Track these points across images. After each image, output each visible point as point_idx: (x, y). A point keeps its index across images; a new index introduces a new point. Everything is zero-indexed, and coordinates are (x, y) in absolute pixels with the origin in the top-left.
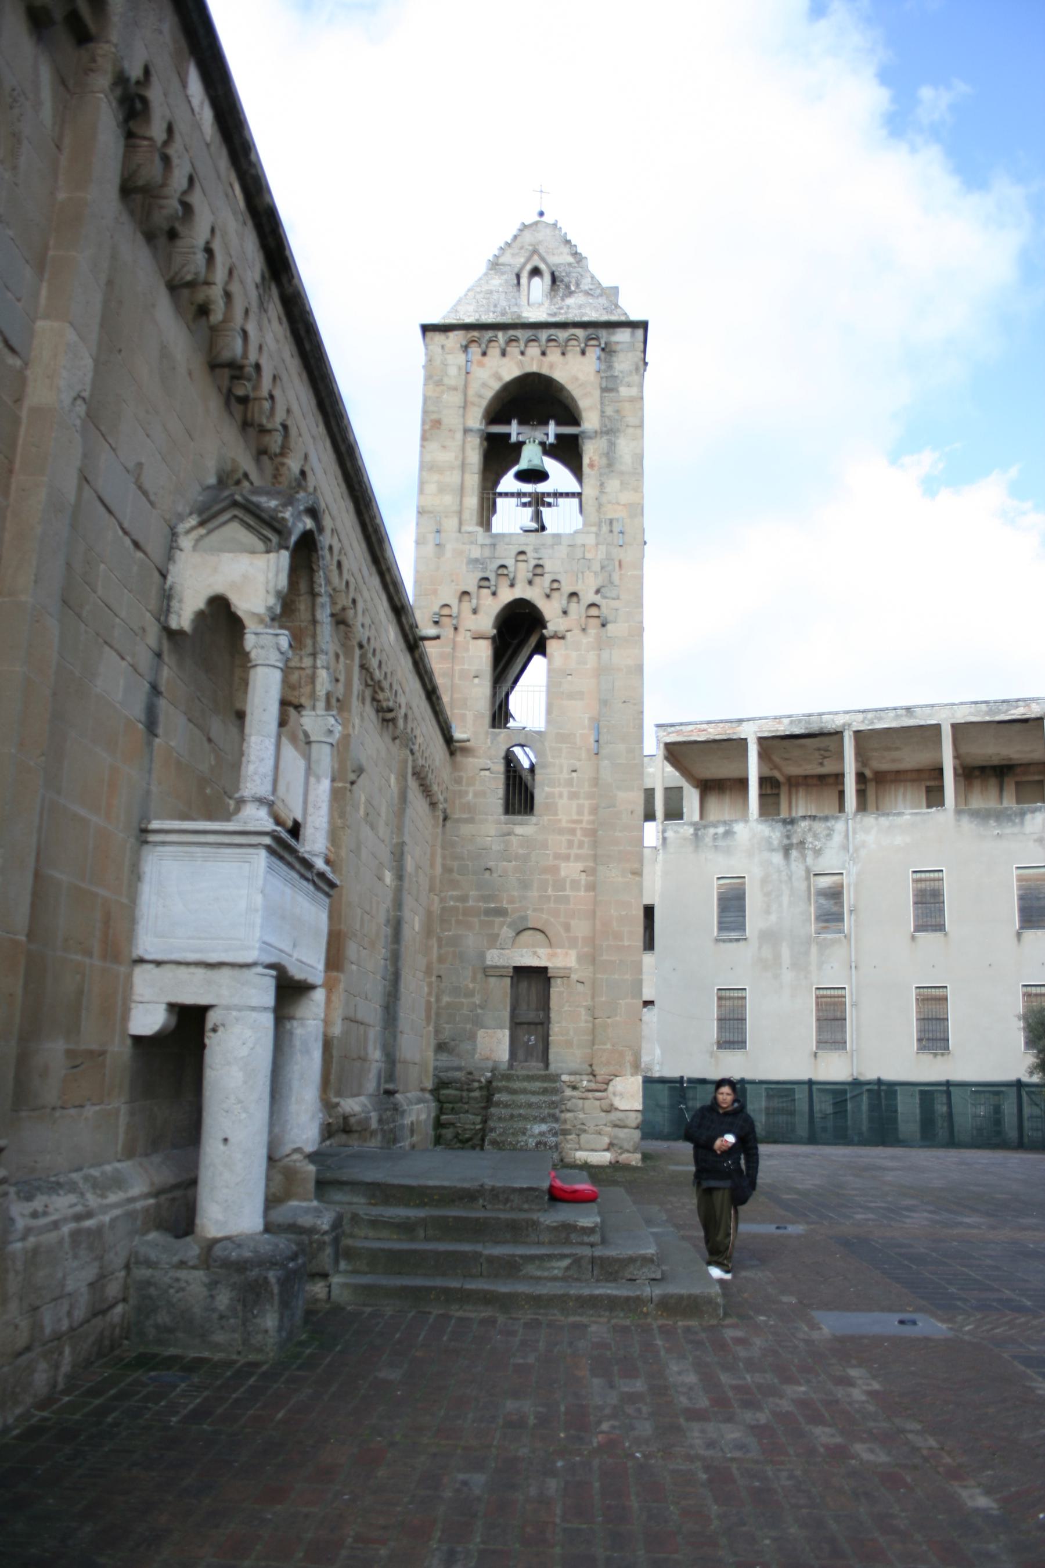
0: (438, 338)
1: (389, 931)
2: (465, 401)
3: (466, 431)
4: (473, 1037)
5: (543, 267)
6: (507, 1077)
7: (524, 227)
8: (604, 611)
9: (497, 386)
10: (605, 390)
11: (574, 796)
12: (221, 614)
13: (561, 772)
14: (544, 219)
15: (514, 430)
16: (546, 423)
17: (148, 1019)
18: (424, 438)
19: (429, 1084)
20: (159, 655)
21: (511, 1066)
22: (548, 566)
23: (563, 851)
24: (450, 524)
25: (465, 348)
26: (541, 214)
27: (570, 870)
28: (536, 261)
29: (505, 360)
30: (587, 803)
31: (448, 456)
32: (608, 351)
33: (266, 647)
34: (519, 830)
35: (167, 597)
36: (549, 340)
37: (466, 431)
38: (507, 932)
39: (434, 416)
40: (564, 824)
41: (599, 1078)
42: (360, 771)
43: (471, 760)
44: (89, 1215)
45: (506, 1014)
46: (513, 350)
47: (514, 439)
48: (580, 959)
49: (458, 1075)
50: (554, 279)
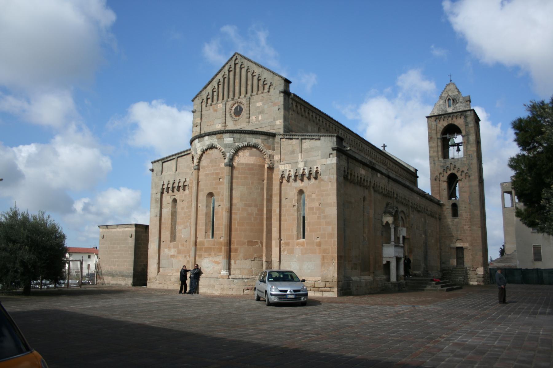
0: (430, 119)
3: (438, 138)
6: (456, 268)
7: (447, 85)
8: (469, 174)
9: (443, 127)
10: (466, 126)
11: (466, 212)
12: (387, 223)
15: (448, 136)
17: (384, 262)
18: (429, 141)
19: (439, 270)
21: (457, 266)
22: (457, 166)
24: (436, 159)
25: (436, 121)
27: (466, 227)
28: (449, 97)
31: (434, 145)
32: (466, 117)
33: (392, 227)
35: (382, 222)
37: (438, 138)
45: (455, 256)
46: (446, 119)
50: (453, 100)
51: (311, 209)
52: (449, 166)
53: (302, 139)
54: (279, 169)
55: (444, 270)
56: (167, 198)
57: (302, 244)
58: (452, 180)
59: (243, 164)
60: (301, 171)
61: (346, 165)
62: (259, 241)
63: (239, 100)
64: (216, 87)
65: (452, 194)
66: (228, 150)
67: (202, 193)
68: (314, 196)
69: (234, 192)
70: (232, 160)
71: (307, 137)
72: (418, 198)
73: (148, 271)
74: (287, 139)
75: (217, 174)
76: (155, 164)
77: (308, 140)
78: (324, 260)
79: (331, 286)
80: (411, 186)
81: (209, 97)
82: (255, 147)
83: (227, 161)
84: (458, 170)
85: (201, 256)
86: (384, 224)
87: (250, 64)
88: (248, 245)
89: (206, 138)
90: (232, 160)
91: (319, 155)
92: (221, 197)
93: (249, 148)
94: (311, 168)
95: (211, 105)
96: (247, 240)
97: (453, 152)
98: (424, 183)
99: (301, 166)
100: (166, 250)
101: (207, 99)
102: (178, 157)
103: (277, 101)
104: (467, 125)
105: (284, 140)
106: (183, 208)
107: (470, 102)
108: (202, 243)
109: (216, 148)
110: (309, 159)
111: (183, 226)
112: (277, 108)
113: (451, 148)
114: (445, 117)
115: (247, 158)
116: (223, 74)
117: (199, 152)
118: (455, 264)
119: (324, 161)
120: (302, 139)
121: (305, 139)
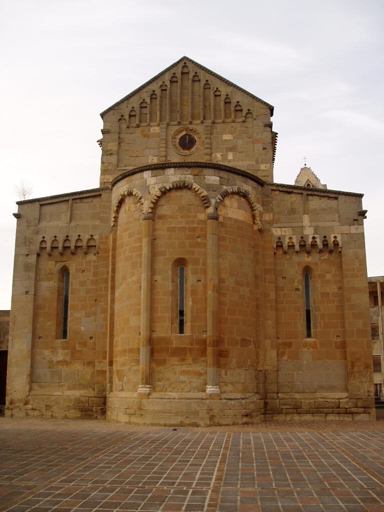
5: (310, 184)
26: (305, 165)
28: (308, 183)
53: (308, 195)
56: (51, 266)
57: (314, 346)
59: (230, 219)
60: (310, 240)
63: (191, 127)
64: (148, 100)
66: (212, 194)
67: (162, 258)
71: (316, 193)
73: (8, 387)
75: (193, 230)
76: (25, 206)
82: (245, 196)
85: (163, 362)
87: (210, 78)
88: (242, 346)
89: (172, 171)
92: (201, 266)
93: (237, 197)
95: (138, 126)
100: (47, 352)
102: (73, 199)
103: (260, 136)
105: (277, 193)
106: (83, 284)
108: (166, 340)
109: (190, 189)
110: (321, 224)
111: (83, 313)
112: (259, 147)
116: (161, 83)
117: (155, 191)
119: (345, 229)
120: (308, 195)
121: (312, 195)
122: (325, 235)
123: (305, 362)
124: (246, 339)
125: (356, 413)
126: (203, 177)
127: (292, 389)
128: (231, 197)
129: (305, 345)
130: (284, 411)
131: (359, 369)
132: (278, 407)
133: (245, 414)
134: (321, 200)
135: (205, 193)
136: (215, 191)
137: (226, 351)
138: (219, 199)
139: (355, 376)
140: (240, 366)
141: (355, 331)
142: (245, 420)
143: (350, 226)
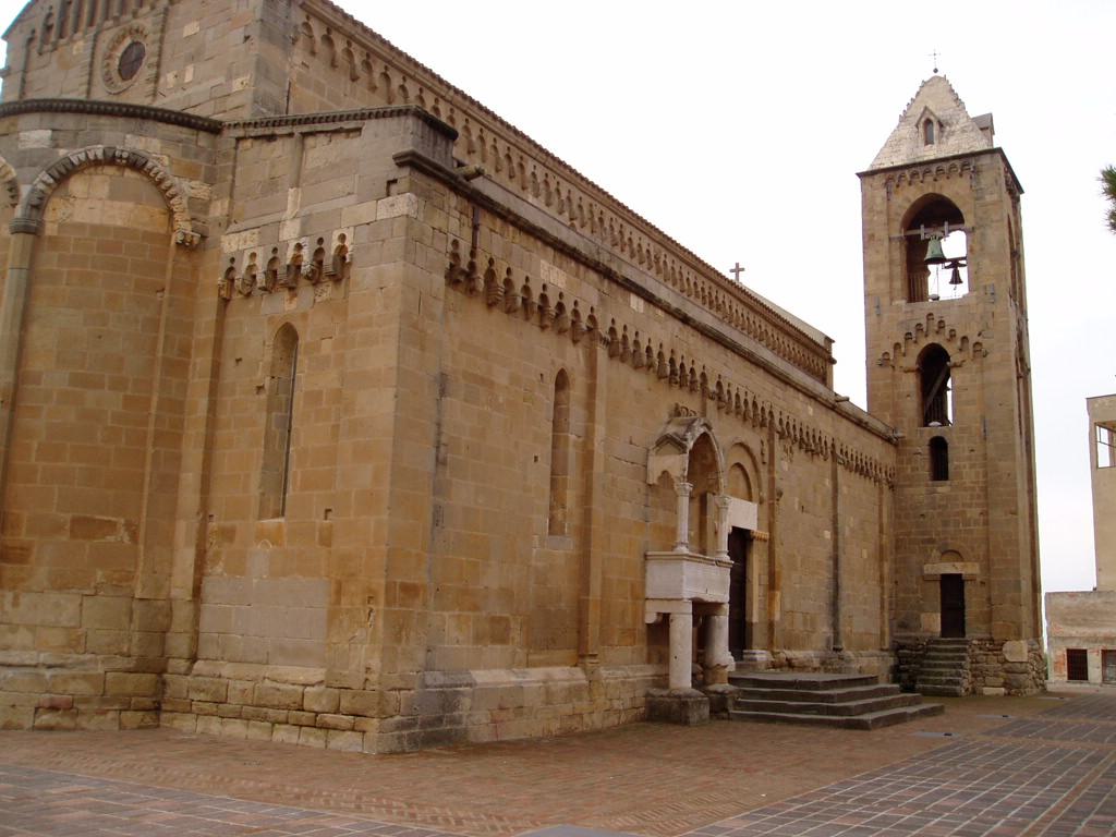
1: (831, 563)
2: (888, 220)
4: (918, 618)
5: (932, 118)
6: (938, 642)
9: (908, 206)
11: (972, 466)
13: (964, 451)
14: (937, 74)
15: (922, 232)
16: (943, 225)
17: (651, 618)
20: (647, 495)
23: (968, 501)
24: (885, 301)
26: (936, 71)
28: (927, 115)
29: (912, 187)
30: (981, 470)
31: (881, 257)
32: (977, 171)
34: (939, 489)
36: (938, 170)
38: (936, 553)
39: (870, 232)
40: (968, 485)
41: (996, 643)
42: (780, 494)
43: (908, 448)
44: (629, 677)
47: (922, 237)
48: (981, 569)
49: (909, 642)
51: (314, 397)
52: (923, 321)
53: (305, 135)
54: (221, 251)
55: (902, 647)
57: (275, 537)
58: (934, 367)
59: (81, 227)
60: (290, 253)
61: (467, 232)
62: (122, 521)
63: (136, 23)
65: (933, 409)
68: (327, 346)
69: (35, 330)
70: (38, 207)
71: (319, 127)
72: (811, 410)
74: (256, 138)
77: (322, 139)
78: (338, 602)
79: (358, 706)
80: (819, 388)
81: (51, 22)
82: (136, 164)
83: (19, 212)
84: (953, 335)
86: (653, 480)
88: (73, 535)
90: (38, 207)
91: (349, 197)
93: (110, 170)
94: (321, 241)
96: (68, 517)
97: (939, 282)
98: (850, 380)
99: (290, 232)
101: (48, 28)
104: (978, 195)
105: (248, 143)
107: (993, 133)
112: (239, 34)
113: (932, 267)
114: (914, 175)
115: (99, 205)
118: (938, 628)
119: (366, 211)
120: (305, 135)
122: (320, 236)
123: (255, 581)
124: (94, 520)
125: (335, 729)
126: (15, 136)
127: (223, 652)
128: (90, 174)
129: (261, 535)
130: (194, 708)
131: (352, 604)
132: (185, 695)
133: (47, 705)
134: (333, 141)
135: (14, 173)
136: (34, 165)
137: (22, 549)
138: (44, 182)
139: (341, 622)
140: (61, 584)
141: (353, 495)
142: (46, 718)
143: (378, 200)
